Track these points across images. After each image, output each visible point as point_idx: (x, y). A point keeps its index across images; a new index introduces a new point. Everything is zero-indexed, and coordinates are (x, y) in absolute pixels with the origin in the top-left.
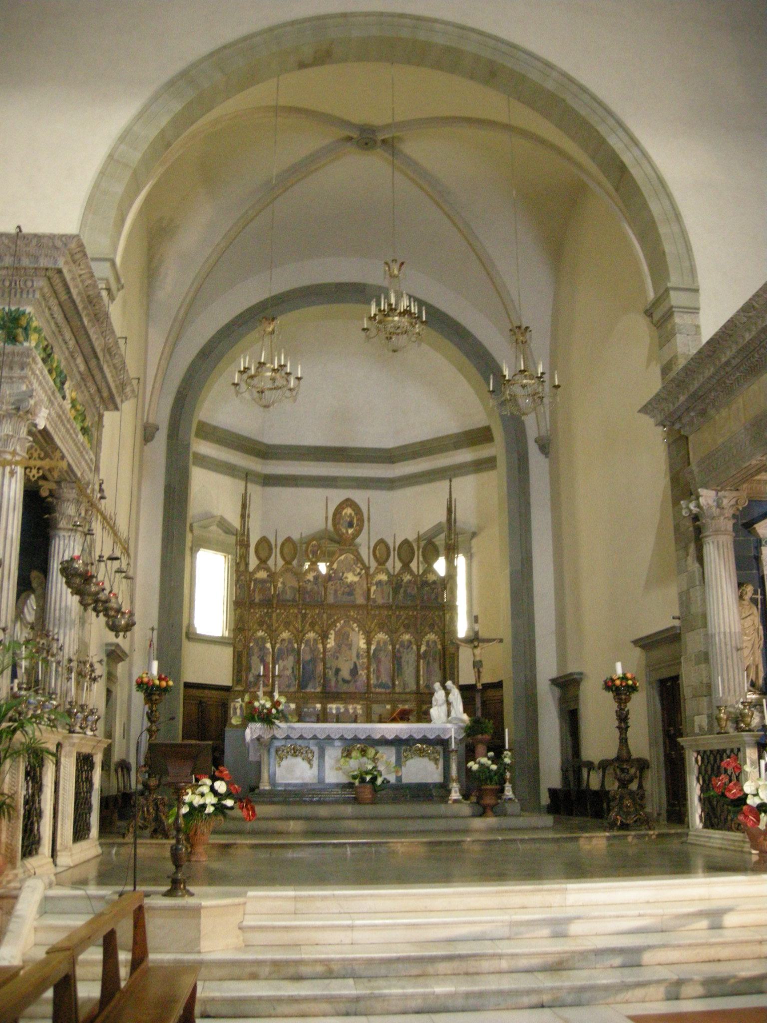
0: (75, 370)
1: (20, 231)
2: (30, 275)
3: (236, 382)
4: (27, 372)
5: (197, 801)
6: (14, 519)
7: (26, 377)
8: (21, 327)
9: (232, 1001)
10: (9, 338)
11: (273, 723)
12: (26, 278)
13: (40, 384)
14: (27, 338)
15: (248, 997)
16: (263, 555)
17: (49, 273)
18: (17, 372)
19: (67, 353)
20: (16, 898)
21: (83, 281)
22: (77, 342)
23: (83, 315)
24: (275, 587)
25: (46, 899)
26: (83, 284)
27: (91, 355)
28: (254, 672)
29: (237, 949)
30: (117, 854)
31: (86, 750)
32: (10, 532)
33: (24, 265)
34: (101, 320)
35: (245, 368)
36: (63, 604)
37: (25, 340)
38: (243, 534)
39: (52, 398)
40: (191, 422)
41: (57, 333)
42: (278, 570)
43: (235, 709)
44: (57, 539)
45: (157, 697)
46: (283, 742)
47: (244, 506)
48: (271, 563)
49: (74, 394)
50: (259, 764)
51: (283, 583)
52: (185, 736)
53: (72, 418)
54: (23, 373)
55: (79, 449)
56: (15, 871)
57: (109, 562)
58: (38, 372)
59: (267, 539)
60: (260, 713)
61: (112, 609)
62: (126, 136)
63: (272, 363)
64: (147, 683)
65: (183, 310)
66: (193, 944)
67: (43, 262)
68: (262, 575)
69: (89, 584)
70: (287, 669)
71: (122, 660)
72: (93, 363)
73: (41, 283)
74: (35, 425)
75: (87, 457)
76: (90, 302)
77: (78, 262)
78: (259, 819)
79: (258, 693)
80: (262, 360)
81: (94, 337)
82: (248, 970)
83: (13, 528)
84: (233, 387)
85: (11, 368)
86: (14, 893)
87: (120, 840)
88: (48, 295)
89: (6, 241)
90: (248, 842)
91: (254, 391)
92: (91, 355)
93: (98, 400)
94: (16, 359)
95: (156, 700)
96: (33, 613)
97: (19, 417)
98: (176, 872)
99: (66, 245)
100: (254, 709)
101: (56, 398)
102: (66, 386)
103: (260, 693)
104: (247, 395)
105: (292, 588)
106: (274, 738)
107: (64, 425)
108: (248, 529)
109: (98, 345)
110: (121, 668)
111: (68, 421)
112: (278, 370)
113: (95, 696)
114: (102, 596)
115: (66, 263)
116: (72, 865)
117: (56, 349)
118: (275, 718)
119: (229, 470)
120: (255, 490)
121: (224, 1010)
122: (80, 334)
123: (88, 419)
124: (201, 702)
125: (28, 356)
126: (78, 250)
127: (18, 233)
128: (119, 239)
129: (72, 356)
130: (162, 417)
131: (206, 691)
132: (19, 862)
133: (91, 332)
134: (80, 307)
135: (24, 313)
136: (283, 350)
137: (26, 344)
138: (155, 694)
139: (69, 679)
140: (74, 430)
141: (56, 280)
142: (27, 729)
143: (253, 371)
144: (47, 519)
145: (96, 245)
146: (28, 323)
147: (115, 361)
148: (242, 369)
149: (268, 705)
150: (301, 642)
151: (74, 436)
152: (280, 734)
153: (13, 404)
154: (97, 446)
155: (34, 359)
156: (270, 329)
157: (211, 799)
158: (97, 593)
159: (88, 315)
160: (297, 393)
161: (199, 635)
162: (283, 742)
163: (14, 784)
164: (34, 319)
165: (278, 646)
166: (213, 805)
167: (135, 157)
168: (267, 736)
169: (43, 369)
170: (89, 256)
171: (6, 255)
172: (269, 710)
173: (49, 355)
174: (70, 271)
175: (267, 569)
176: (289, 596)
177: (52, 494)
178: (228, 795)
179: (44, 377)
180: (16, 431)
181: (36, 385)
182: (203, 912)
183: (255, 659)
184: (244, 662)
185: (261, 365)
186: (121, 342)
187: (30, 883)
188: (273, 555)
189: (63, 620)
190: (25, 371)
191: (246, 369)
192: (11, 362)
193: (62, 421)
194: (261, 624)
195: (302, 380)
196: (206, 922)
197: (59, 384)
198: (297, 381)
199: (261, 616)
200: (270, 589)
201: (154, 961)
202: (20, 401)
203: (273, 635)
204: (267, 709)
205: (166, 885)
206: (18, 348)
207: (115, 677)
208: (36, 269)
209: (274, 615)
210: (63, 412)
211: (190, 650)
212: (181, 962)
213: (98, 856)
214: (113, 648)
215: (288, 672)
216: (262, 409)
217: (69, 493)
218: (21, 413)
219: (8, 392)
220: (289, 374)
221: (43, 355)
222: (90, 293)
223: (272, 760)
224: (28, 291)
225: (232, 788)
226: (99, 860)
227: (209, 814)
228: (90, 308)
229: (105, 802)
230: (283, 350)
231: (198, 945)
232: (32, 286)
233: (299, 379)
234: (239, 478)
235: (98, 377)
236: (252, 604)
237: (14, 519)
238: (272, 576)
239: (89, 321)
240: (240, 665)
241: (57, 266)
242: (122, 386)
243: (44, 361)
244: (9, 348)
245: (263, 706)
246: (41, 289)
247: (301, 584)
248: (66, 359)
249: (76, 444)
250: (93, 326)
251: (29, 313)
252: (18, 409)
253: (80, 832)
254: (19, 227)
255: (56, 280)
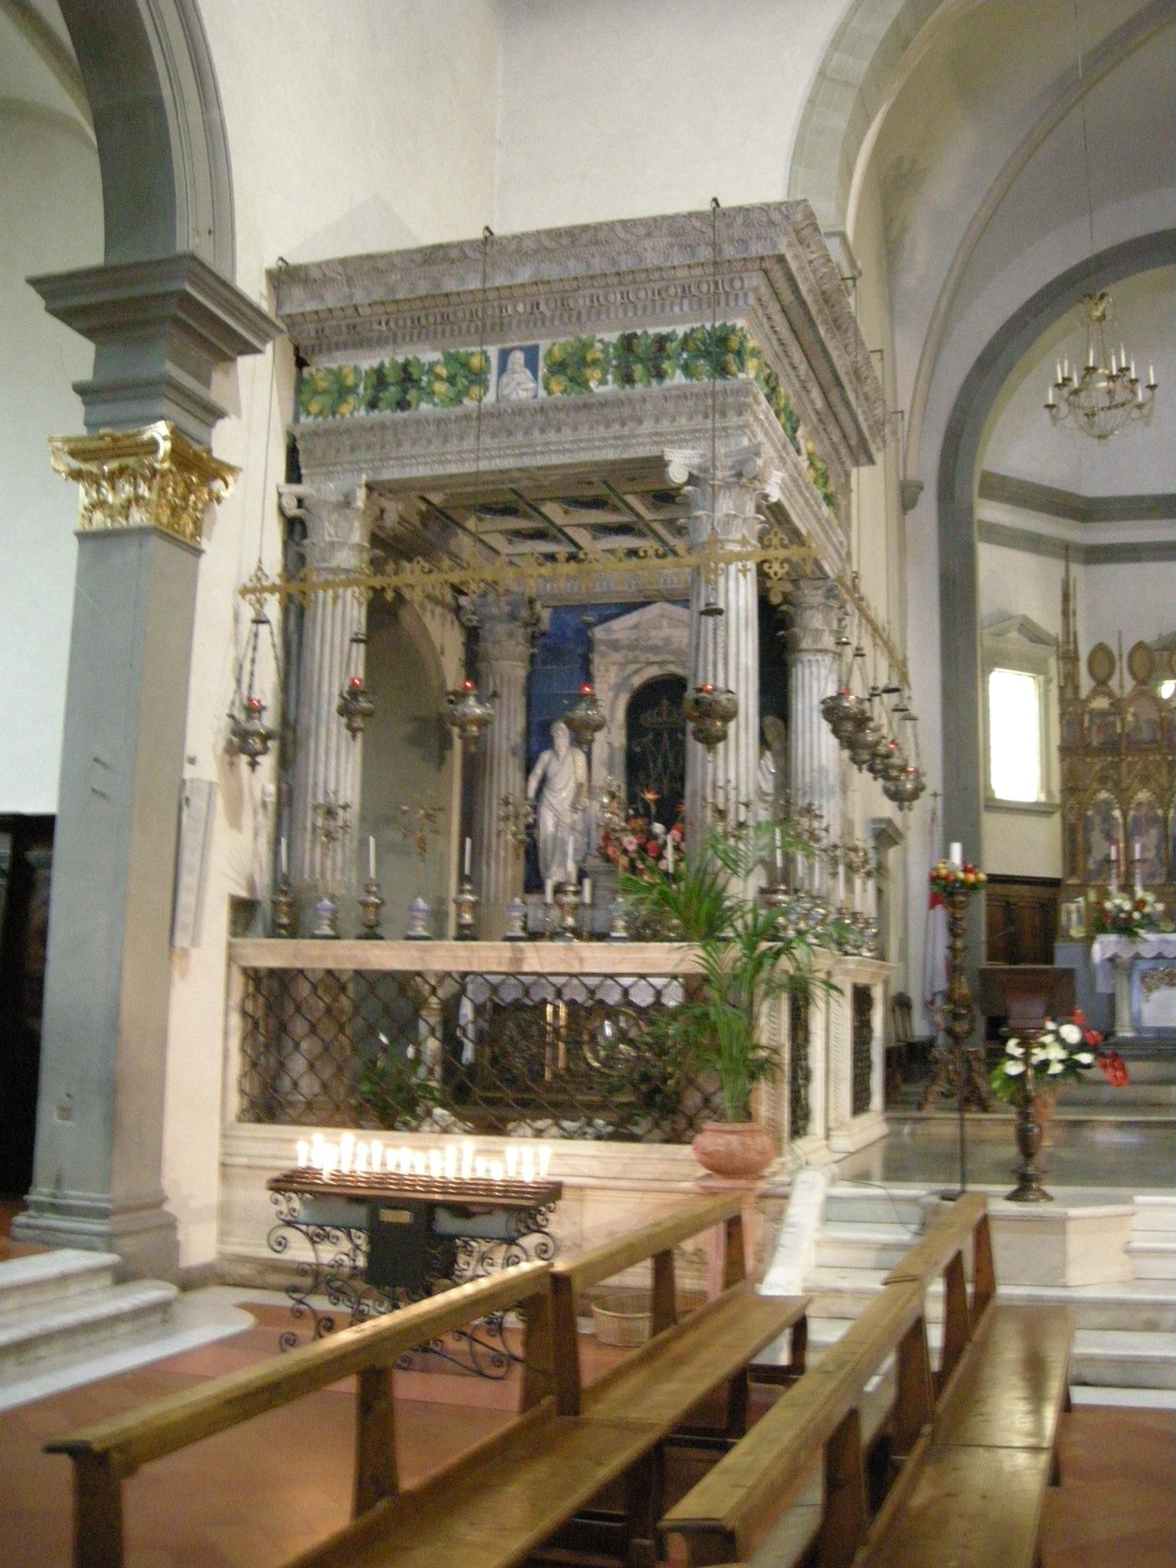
0: (809, 407)
1: (718, 205)
2: (736, 272)
3: (1051, 402)
4: (748, 417)
5: (1039, 1055)
6: (746, 642)
7: (747, 425)
8: (732, 352)
9: (1121, 1362)
10: (716, 370)
11: (1136, 934)
12: (731, 276)
13: (767, 434)
14: (742, 367)
15: (1145, 1357)
16: (1101, 672)
17: (767, 265)
18: (733, 420)
19: (797, 385)
20: (785, 1197)
21: (814, 272)
22: (811, 366)
23: (818, 321)
24: (1123, 721)
25: (830, 1199)
26: (815, 276)
27: (831, 383)
28: (1097, 855)
29: (1123, 1283)
30: (912, 1134)
31: (862, 980)
32: (743, 660)
33: (728, 257)
34: (844, 327)
35: (1064, 379)
36: (816, 762)
37: (740, 371)
38: (1068, 642)
39: (785, 455)
40: (971, 474)
41: (781, 354)
42: (1125, 695)
43: (1069, 913)
44: (800, 667)
45: (962, 898)
46: (1151, 964)
47: (1066, 598)
48: (1113, 683)
49: (810, 446)
50: (1111, 999)
51: (1135, 715)
52: (992, 957)
53: (811, 480)
54: (740, 421)
55: (824, 529)
56: (783, 1159)
57: (885, 696)
58: (762, 417)
59: (1106, 646)
60: (1116, 919)
61: (893, 767)
62: (840, 40)
63: (1107, 366)
64: (946, 878)
65: (944, 304)
66: (1057, 1274)
67: (757, 249)
68: (1101, 703)
69: (863, 731)
70: (1149, 849)
71: (894, 842)
72: (834, 396)
73: (755, 280)
74: (766, 497)
75: (835, 539)
76: (826, 301)
77: (806, 243)
78: (1133, 1083)
79: (1110, 888)
80: (1091, 364)
81: (834, 355)
82: (1144, 1315)
83: (747, 653)
84: (1047, 410)
85: (724, 415)
86: (782, 1190)
87: (916, 1114)
88: (765, 298)
89: (698, 224)
90: (1112, 1118)
91: (1080, 413)
92: (831, 383)
93: (843, 450)
94: (730, 400)
95: (962, 902)
96: (770, 778)
97: (742, 486)
98: (1026, 1165)
99: (787, 218)
100: (1104, 913)
101: (788, 454)
102: (800, 433)
103: (1113, 888)
104: (1069, 422)
105: (1149, 721)
106: (1137, 957)
107: (801, 493)
108: (1075, 635)
109: (841, 364)
110: (893, 855)
111: (807, 487)
112: (1117, 376)
113: (864, 899)
114: (882, 750)
115: (790, 245)
116: (852, 1150)
117: (782, 380)
118: (1137, 926)
119: (1033, 543)
120: (1077, 570)
121: (1109, 1375)
122: (816, 354)
123: (831, 481)
124: (1008, 904)
125: (747, 393)
126: (807, 222)
127: (714, 209)
128: (847, 199)
129: (805, 388)
130: (926, 466)
131: (1016, 887)
132: (786, 1147)
133: (830, 346)
134: (814, 311)
135: (733, 329)
136: (1122, 345)
137: (742, 376)
138: (957, 894)
139: (835, 875)
140: (815, 499)
141: (777, 274)
142: (796, 952)
143: (1076, 384)
144: (783, 636)
145: (824, 211)
146: (741, 343)
147: (866, 389)
148: (1060, 381)
149: (1127, 906)
150: (1169, 807)
151: (816, 508)
152: (1147, 951)
153: (732, 468)
154: (845, 523)
155: (755, 397)
156: (1097, 313)
157: (1056, 1053)
158: (877, 743)
159: (825, 322)
160: (1151, 411)
161: (1001, 801)
162: (1151, 964)
163: (775, 1033)
164: (749, 336)
165: (1132, 813)
166: (1061, 1061)
167: (859, 67)
168: (1126, 955)
169: (769, 412)
170: (822, 231)
171: (699, 244)
172: (1130, 914)
173: (774, 390)
174: (796, 257)
175: (1109, 694)
176: (1146, 734)
177: (787, 599)
178: (1082, 1047)
179: (770, 423)
180: (740, 508)
181: (761, 437)
182: (1071, 1226)
183: (1096, 837)
184: (1080, 839)
185: (1090, 370)
186: (875, 358)
187: (803, 1176)
188: (1117, 671)
189: (817, 787)
190: (744, 418)
191: (1067, 380)
192: (724, 404)
193: (798, 487)
194: (1103, 780)
195: (1159, 388)
196: (1076, 1242)
197: (790, 432)
198: (1149, 392)
199: (1103, 768)
200: (1113, 725)
201: (1010, 1297)
202: (742, 462)
203: (1123, 797)
204: (1125, 912)
205: (1010, 1183)
206: (730, 383)
207: (887, 870)
208: (745, 259)
209: (1124, 767)
210: (800, 475)
211: (991, 823)
212: (1039, 1299)
213: (884, 1137)
214: (883, 826)
215: (1151, 855)
216: (1096, 441)
217: (812, 595)
218: (744, 480)
219: (723, 451)
220: (1134, 382)
221: (766, 390)
222: (827, 287)
223: (1135, 992)
224: (737, 295)
225: (1087, 1035)
226: (884, 1142)
227: (1054, 1076)
228: (826, 310)
229: (889, 1055)
230: (1122, 345)
231: (1063, 1276)
232: (742, 287)
233: (1151, 387)
234: (1054, 555)
235: (843, 415)
236: (1088, 750)
237: (746, 642)
238: (1117, 706)
239: (827, 330)
240: (1074, 844)
241: (777, 252)
242: (878, 426)
243: (768, 398)
244: (720, 383)
245: (1120, 910)
246: (756, 290)
247: (1163, 714)
248: (796, 392)
249: (819, 520)
250: (832, 338)
251: (742, 329)
252: (739, 475)
253: (860, 1102)
254: (715, 200)
255: (777, 274)
